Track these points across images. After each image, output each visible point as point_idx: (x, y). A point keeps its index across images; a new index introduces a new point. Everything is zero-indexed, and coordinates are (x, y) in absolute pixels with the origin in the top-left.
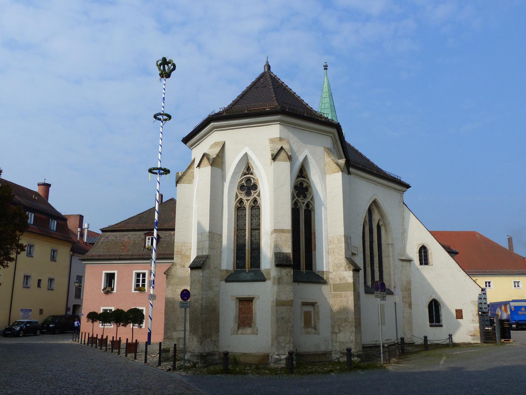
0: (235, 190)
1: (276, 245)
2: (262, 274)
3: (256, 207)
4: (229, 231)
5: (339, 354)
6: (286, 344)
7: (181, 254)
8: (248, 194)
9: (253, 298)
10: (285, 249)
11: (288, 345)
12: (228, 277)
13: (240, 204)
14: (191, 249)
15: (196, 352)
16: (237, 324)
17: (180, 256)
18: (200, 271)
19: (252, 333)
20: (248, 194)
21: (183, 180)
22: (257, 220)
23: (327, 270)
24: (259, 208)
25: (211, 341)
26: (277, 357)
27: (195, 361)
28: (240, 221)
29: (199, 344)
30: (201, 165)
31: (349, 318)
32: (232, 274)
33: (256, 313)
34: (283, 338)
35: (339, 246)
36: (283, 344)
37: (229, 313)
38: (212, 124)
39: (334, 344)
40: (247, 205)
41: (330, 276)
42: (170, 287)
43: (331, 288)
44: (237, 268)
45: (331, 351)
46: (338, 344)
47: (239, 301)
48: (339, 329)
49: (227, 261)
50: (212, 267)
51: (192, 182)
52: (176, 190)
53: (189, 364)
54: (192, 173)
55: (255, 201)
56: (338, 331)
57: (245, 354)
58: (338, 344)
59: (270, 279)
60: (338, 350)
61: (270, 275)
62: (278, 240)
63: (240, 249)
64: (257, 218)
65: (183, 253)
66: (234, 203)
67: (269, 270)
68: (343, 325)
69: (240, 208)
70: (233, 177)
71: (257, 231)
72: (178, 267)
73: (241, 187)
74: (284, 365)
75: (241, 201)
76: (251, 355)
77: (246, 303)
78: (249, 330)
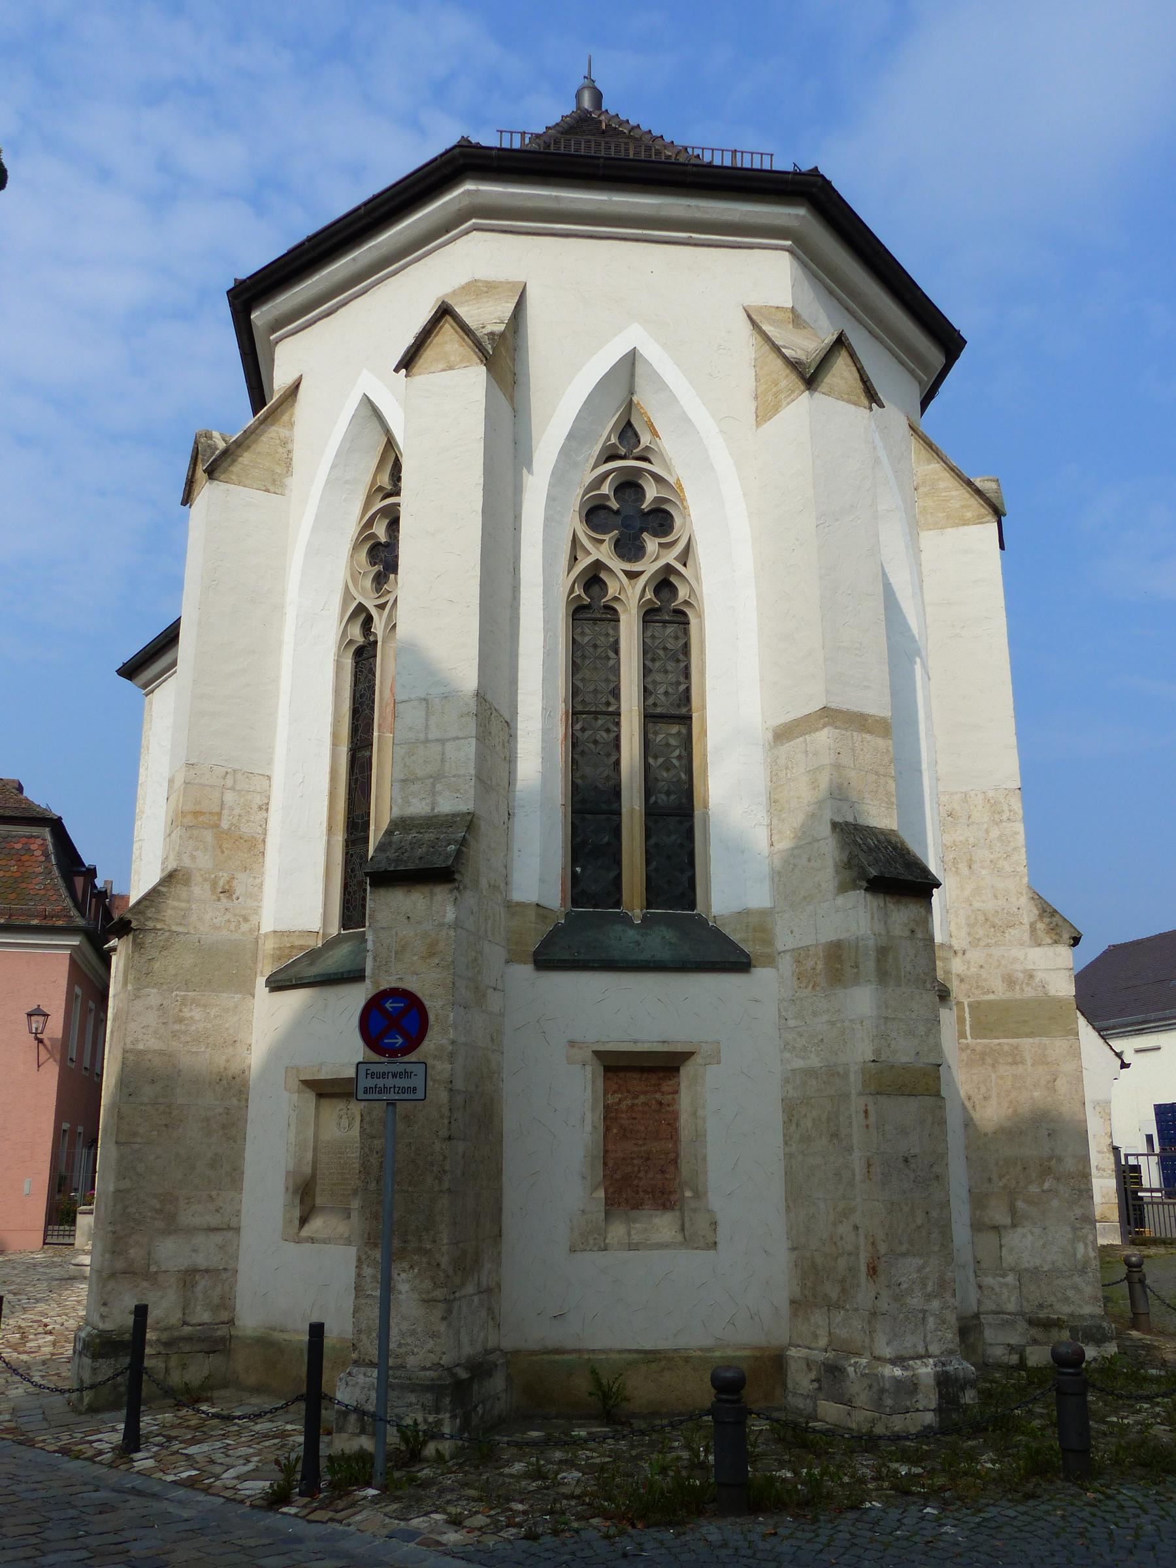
0: (572, 522)
1: (840, 787)
2: (718, 936)
3: (669, 612)
4: (547, 712)
5: (1022, 1325)
6: (929, 1297)
7: (217, 826)
8: (629, 548)
9: (686, 1056)
10: (873, 811)
11: (936, 1304)
12: (548, 941)
13: (587, 587)
14: (264, 807)
15: (411, 1361)
16: (601, 1194)
17: (208, 836)
18: (441, 894)
19: (688, 1239)
20: (629, 548)
21: (236, 468)
22: (671, 677)
23: (946, 940)
24: (680, 619)
25: (951, 1352)
26: (898, 1372)
27: (415, 1416)
28: (587, 673)
29: (438, 1312)
30: (429, 354)
31: (1060, 1160)
32: (557, 931)
33: (700, 1137)
34: (914, 1262)
35: (995, 833)
36: (915, 1301)
37: (555, 1131)
38: (469, 186)
39: (989, 1280)
40: (629, 596)
41: (957, 966)
42: (153, 996)
43: (961, 1020)
44: (575, 902)
45: (977, 1316)
46: (1010, 1279)
47: (607, 1069)
48: (1013, 1211)
49: (534, 864)
50: (484, 882)
51: (283, 486)
52: (185, 519)
53: (366, 1443)
54: (284, 443)
55: (665, 583)
56: (1008, 1221)
57: (651, 1357)
58: (1010, 1279)
59: (770, 961)
60: (1011, 1307)
61: (769, 942)
62: (845, 760)
63: (591, 808)
64: (670, 666)
65: (225, 825)
66: (564, 582)
67: (763, 913)
68: (1034, 1189)
69: (589, 609)
70: (565, 452)
71: (675, 729)
72: (197, 891)
73: (595, 514)
74: (929, 1418)
75: (593, 579)
76: (687, 1360)
77: (642, 1079)
78: (663, 1225)
